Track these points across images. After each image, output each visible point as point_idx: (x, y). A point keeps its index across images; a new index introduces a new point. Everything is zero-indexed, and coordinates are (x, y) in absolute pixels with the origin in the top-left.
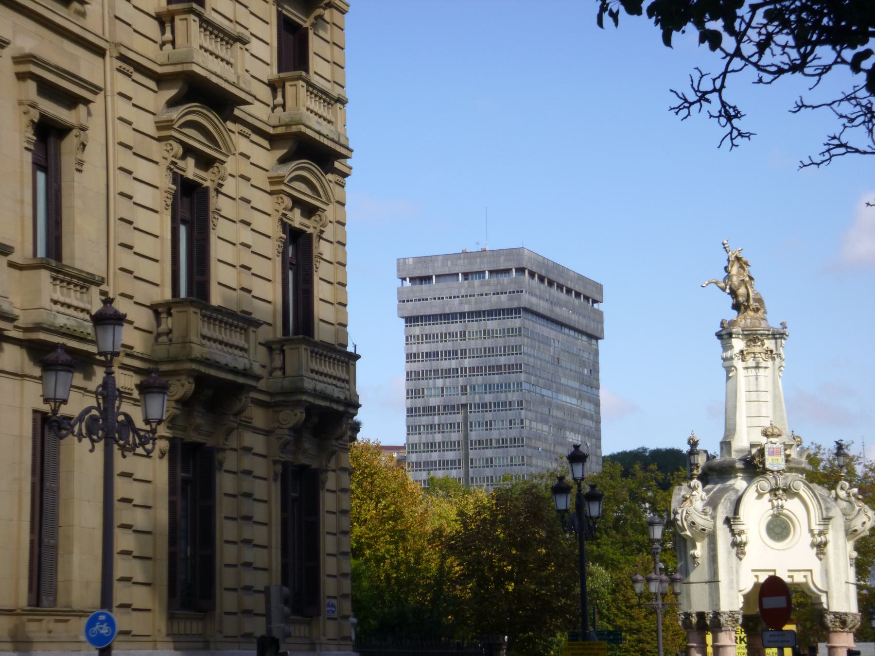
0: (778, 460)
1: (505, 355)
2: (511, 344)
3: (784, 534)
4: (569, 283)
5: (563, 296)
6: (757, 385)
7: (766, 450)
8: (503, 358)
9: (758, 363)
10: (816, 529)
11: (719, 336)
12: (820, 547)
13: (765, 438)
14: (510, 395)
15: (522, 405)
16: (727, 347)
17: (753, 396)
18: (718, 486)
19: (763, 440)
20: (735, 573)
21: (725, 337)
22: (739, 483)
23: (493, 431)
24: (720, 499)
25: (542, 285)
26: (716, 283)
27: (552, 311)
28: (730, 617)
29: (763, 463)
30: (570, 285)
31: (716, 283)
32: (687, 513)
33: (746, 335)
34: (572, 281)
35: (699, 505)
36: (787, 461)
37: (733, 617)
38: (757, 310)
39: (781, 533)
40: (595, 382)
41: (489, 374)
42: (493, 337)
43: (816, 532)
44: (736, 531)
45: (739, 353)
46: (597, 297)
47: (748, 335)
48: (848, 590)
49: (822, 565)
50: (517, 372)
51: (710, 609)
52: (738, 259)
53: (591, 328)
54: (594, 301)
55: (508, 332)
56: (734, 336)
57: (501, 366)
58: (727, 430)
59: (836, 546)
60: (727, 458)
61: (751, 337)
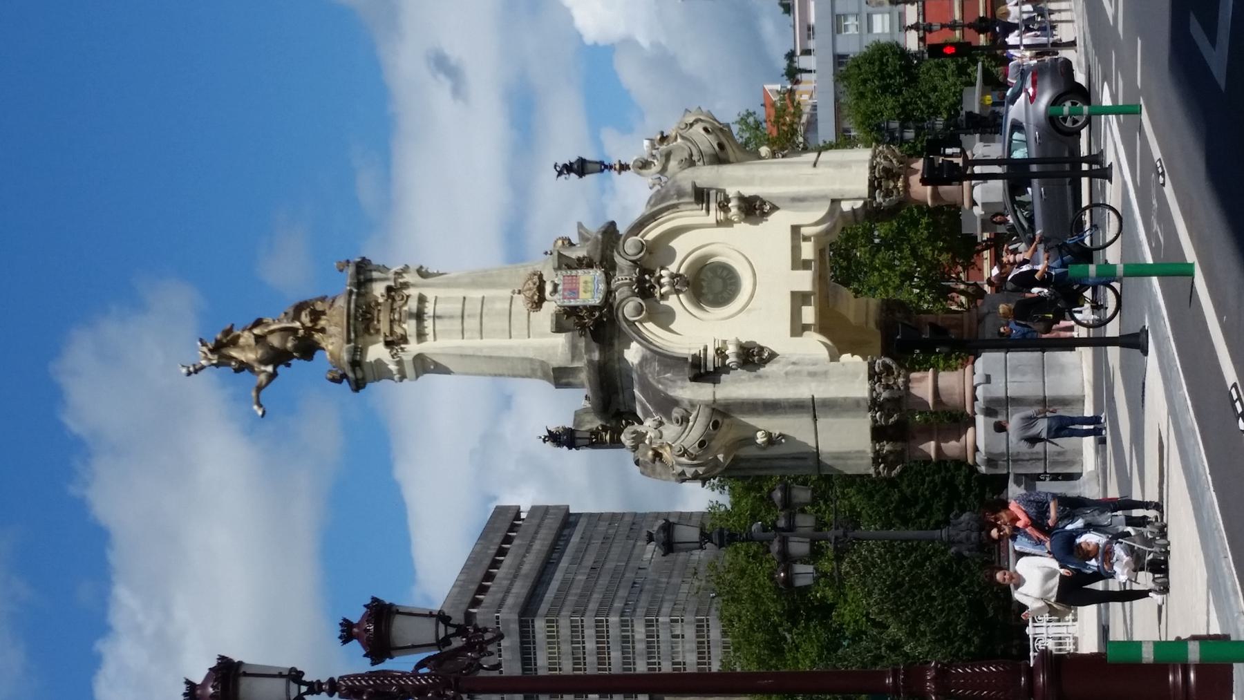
0: (586, 282)
1: (584, 643)
2: (569, 633)
3: (725, 273)
4: (490, 552)
5: (507, 561)
6: (451, 317)
7: (567, 303)
8: (587, 645)
9: (410, 315)
10: (715, 214)
11: (358, 385)
12: (754, 209)
13: (545, 305)
14: (638, 637)
15: (652, 621)
16: (380, 372)
17: (471, 323)
18: (637, 392)
19: (550, 308)
20: (798, 369)
21: (360, 375)
22: (633, 354)
23: (687, 661)
24: (659, 391)
25: (491, 589)
26: (259, 389)
27: (526, 576)
28: (879, 380)
29: (591, 309)
30: (493, 550)
31: (259, 389)
32: (682, 455)
33: (356, 336)
34: (489, 549)
35: (671, 430)
36: (590, 265)
37: (881, 373)
38: (316, 315)
39: (722, 278)
40: (626, 519)
41: (610, 664)
42: (559, 658)
43: (721, 216)
44: (719, 363)
45: (392, 349)
46: (511, 515)
47: (355, 332)
48: (829, 164)
49: (786, 208)
50: (607, 626)
51: (865, 417)
52: (218, 348)
53: (552, 524)
54: (518, 517)
55: (553, 637)
56: (358, 357)
57: (598, 648)
58: (532, 375)
59: (748, 182)
60: (583, 376)
61: (361, 327)
